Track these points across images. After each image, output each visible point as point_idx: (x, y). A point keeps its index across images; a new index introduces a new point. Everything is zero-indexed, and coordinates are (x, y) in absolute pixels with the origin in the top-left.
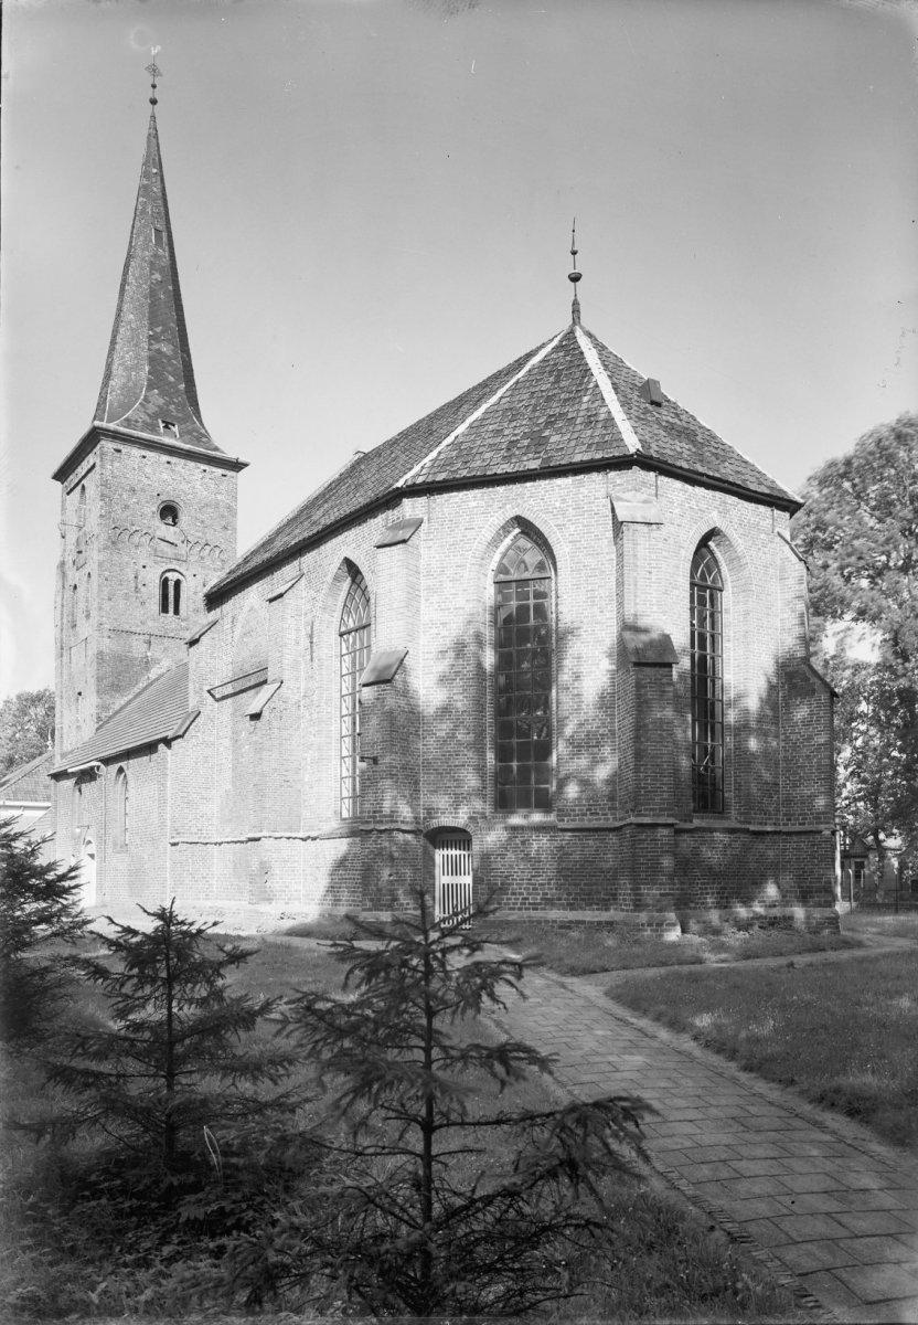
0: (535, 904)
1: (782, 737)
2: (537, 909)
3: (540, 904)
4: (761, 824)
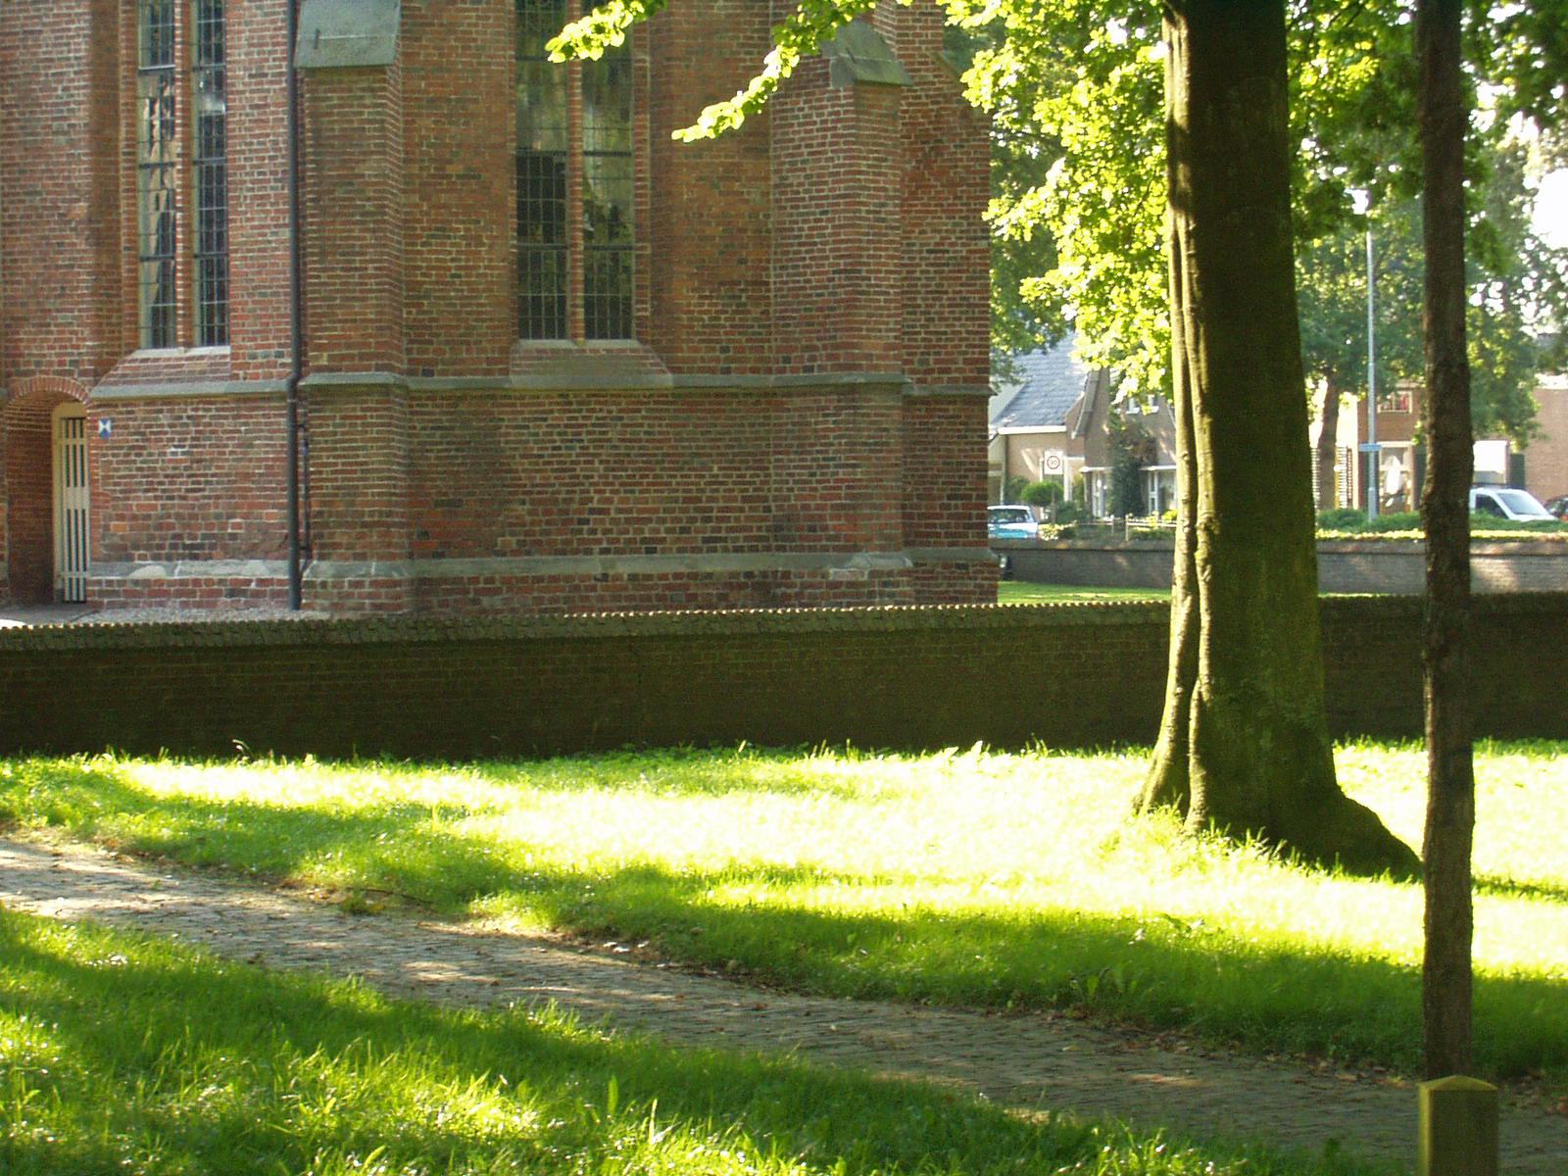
0: (192, 547)
1: (774, 180)
2: (195, 557)
3: (201, 547)
4: (754, 370)
